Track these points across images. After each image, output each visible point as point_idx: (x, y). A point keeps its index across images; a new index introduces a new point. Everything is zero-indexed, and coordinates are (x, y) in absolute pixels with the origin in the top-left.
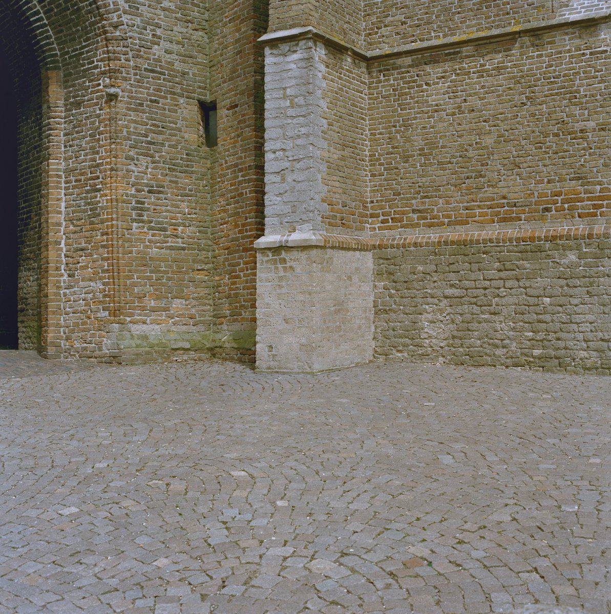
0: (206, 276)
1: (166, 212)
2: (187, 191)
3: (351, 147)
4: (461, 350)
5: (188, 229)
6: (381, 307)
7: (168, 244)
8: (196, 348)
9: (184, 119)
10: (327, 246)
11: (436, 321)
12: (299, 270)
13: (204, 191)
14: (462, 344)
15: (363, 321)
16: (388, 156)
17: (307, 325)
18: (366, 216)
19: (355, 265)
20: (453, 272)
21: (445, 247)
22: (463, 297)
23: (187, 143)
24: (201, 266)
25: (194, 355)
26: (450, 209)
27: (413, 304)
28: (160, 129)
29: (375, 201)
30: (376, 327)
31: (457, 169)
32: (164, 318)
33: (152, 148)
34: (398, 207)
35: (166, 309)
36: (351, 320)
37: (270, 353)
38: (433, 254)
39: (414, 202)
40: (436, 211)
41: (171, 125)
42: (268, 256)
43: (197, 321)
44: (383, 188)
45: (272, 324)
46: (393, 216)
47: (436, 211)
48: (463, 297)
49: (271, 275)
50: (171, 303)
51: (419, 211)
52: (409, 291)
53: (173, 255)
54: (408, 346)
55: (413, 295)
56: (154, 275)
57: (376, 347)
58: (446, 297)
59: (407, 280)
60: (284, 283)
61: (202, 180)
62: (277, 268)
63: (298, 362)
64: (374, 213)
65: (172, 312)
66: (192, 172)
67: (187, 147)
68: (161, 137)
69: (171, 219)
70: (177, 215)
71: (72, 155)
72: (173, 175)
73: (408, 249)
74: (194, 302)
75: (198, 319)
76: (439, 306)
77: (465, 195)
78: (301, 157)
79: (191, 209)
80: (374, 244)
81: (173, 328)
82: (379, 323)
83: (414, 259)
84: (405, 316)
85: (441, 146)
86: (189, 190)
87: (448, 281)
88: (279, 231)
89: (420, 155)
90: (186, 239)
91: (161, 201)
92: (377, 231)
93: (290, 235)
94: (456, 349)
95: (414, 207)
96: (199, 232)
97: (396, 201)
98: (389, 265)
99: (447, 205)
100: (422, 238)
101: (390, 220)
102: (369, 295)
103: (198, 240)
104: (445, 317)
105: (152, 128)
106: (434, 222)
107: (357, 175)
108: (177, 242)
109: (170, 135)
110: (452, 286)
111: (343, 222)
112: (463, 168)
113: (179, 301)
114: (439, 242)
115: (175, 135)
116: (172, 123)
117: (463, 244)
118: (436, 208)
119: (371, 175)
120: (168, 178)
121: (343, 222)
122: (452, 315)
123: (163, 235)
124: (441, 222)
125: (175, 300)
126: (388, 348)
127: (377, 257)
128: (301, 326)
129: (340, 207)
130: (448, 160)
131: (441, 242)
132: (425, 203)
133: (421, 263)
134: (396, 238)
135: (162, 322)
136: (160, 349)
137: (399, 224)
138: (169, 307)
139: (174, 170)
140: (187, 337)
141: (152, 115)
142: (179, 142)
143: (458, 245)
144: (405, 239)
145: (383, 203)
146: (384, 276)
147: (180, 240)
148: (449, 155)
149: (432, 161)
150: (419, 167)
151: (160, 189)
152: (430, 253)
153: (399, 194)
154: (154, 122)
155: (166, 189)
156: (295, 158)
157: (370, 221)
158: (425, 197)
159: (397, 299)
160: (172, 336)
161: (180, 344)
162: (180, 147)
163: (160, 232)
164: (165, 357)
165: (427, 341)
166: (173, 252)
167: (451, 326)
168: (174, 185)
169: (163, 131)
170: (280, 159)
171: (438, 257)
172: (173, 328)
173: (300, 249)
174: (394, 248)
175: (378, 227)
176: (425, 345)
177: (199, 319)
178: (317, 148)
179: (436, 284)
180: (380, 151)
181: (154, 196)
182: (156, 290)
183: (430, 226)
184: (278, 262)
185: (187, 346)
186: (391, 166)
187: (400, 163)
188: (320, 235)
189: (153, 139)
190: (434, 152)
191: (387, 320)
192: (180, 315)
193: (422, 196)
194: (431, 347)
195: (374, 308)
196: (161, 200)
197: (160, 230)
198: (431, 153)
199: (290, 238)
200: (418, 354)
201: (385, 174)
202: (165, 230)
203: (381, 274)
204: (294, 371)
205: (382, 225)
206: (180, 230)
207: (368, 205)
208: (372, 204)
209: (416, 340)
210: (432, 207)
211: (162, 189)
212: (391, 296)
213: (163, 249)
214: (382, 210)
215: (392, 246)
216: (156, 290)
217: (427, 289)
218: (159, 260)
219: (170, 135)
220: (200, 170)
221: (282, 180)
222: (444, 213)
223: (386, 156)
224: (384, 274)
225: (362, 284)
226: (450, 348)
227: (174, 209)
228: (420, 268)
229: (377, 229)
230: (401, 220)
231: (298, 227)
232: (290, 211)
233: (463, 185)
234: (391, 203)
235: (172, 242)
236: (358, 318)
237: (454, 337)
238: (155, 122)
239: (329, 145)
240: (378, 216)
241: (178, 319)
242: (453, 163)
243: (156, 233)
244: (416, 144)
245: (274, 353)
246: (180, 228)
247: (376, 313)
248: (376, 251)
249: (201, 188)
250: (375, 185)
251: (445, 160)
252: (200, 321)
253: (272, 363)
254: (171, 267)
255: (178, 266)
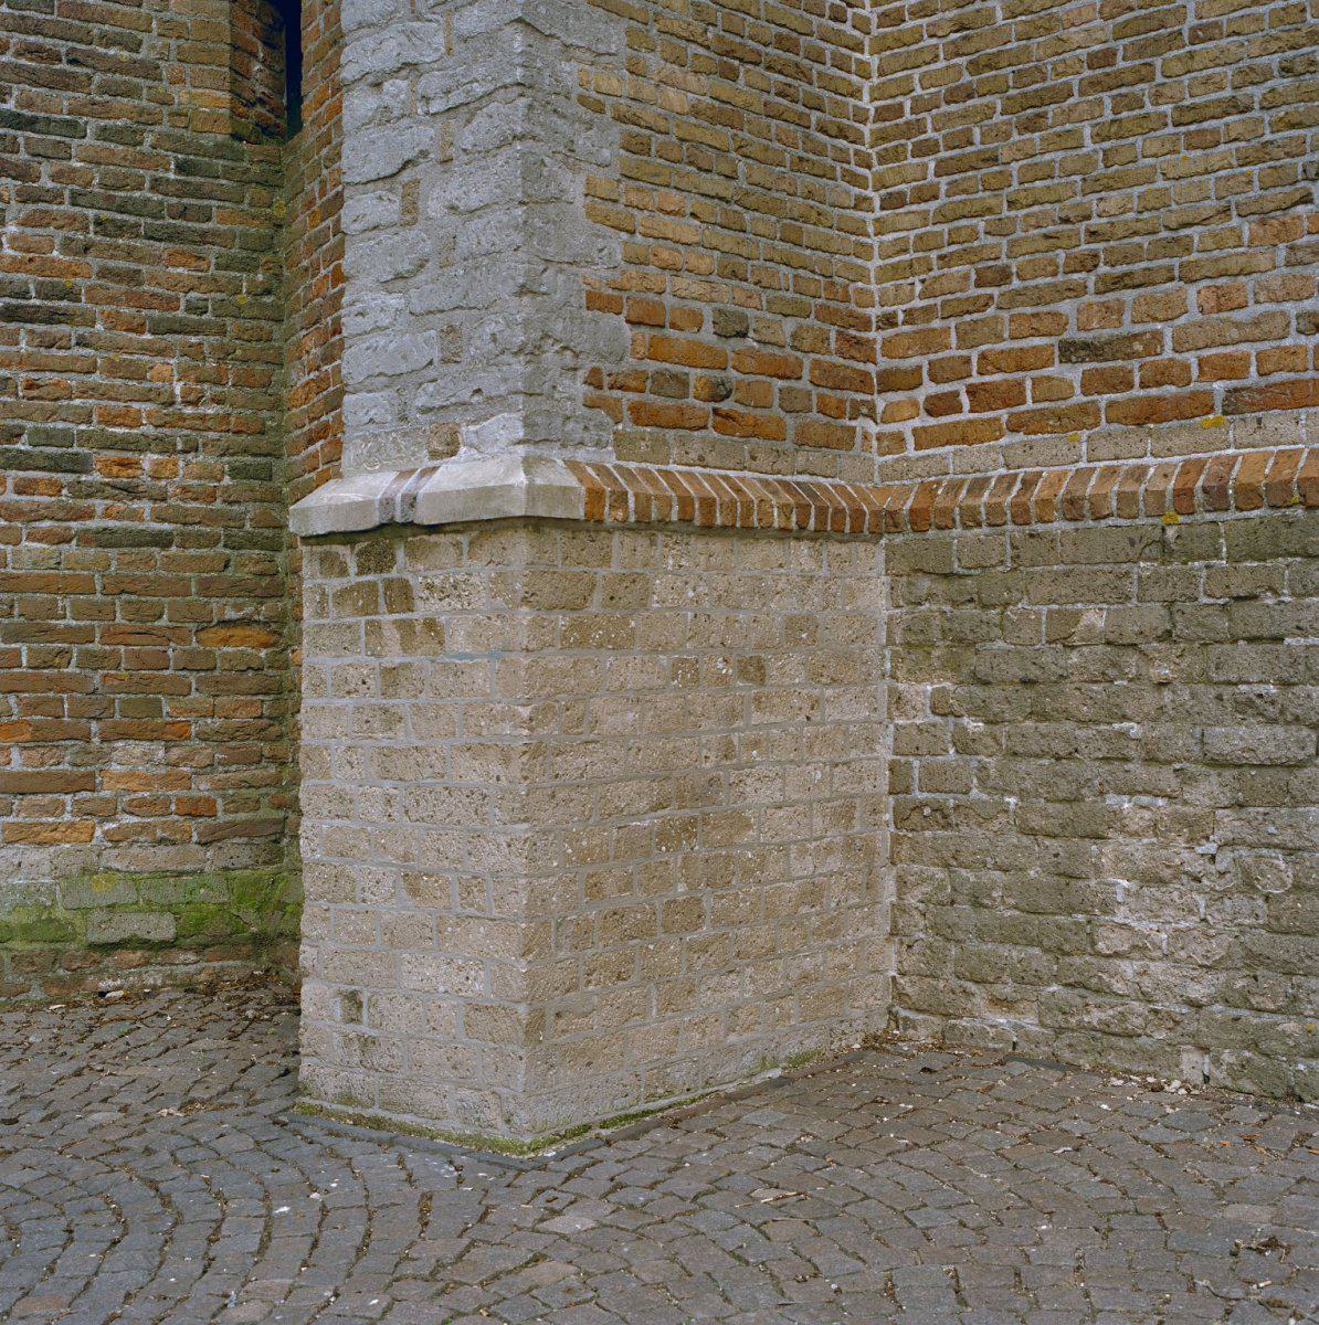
0: (265, 645)
1: (83, 394)
2: (180, 314)
3: (769, 68)
4: (1290, 1026)
5: (181, 464)
6: (922, 796)
7: (92, 524)
8: (201, 939)
9: (170, 29)
10: (608, 520)
11: (1167, 873)
12: (460, 636)
13: (256, 312)
14: (1295, 998)
15: (834, 863)
16: (953, 107)
17: (495, 913)
18: (863, 382)
19: (783, 607)
20: (1251, 640)
21: (1209, 517)
22: (1300, 765)
23: (182, 121)
24: (238, 607)
25: (192, 968)
26: (1235, 333)
27: (1064, 789)
28: (64, 66)
29: (901, 317)
30: (902, 882)
31: (1268, 137)
32: (67, 817)
33: (21, 140)
34: (1000, 338)
35: (87, 783)
36: (762, 867)
37: (350, 1028)
38: (1155, 551)
39: (1066, 307)
40: (1169, 343)
41: (112, 52)
42: (343, 572)
43: (220, 827)
44: (934, 255)
45: (358, 895)
46: (976, 379)
47: (1169, 343)
48: (1300, 765)
49: (359, 662)
50: (104, 757)
51: (1092, 350)
52: (1042, 726)
53: (114, 563)
54: (1038, 980)
55: (1059, 747)
56: (25, 648)
57: (903, 974)
58: (1217, 763)
59: (1034, 672)
60: (401, 703)
61: (248, 266)
62: (375, 629)
63: (459, 1086)
64: (898, 370)
65: (106, 794)
66: (204, 240)
67: (180, 139)
68: (64, 100)
69: (107, 423)
70: (136, 406)
71: (809, 394)
72: (117, 247)
73: (1040, 528)
74: (205, 753)
75: (222, 817)
76: (1185, 803)
77: (1308, 258)
78: (479, 89)
79: (199, 381)
80: (895, 507)
81: (112, 858)
82: (916, 867)
83: (1067, 574)
84: (1026, 840)
85: (1193, 30)
86: (190, 308)
87: (1229, 683)
88: (394, 454)
89: (1095, 84)
90: (172, 501)
91: (61, 353)
92: (911, 452)
93: (435, 469)
94: (1266, 1018)
95: (1071, 333)
96: (235, 472)
97: (991, 311)
98: (954, 603)
99: (1224, 315)
100: (1102, 476)
101: (965, 400)
102: (870, 741)
103: (231, 503)
104: (1213, 858)
105: (23, 61)
106: (1160, 399)
107: (810, 195)
108: (135, 515)
109: (104, 89)
110: (1246, 706)
111: (725, 406)
112: (1299, 125)
113: (137, 748)
114: (1184, 494)
115: (131, 92)
116: (115, 43)
117: (1297, 497)
118: (1168, 333)
119: (882, 200)
120: (93, 261)
121: (725, 406)
122: (1244, 852)
123: (70, 486)
124: (1194, 395)
125: (120, 744)
126: (954, 982)
127: (904, 567)
128: (471, 911)
129: (707, 335)
130: (1227, 93)
131: (1189, 493)
132: (1120, 312)
133: (1094, 596)
134: (988, 480)
135: (57, 835)
136: (37, 946)
137: (1003, 414)
138: (92, 775)
139: (121, 229)
140: (171, 892)
141: (27, 13)
142: (146, 120)
143: (1273, 507)
144: (1028, 484)
145: (936, 324)
146: (936, 653)
147: (145, 506)
148: (1229, 71)
149: (1149, 108)
150: (1089, 146)
151: (57, 303)
152: (1138, 547)
153: (1003, 276)
154: (32, 39)
155: (84, 304)
156: (455, 99)
157: (880, 405)
158: (1119, 282)
159: (991, 762)
160: (102, 892)
161: (133, 925)
162: (149, 139)
163: (55, 476)
164: (60, 979)
165: (1128, 968)
166: (112, 553)
167: (1240, 901)
168: (124, 287)
169: (74, 76)
170: (396, 113)
171: (1176, 565)
172: (112, 858)
173: (463, 539)
174: (979, 525)
175: (915, 431)
176: (1118, 987)
177: (231, 817)
178: (554, 45)
179: (1167, 695)
180: (919, 91)
181: (32, 332)
182: (32, 707)
183: (1145, 415)
184: (381, 600)
185: (164, 928)
186: (970, 149)
187: (1008, 135)
188: (573, 466)
189: (30, 105)
190: (1158, 62)
191: (947, 855)
192: (142, 803)
193: (1101, 279)
194: (1147, 998)
195: (891, 799)
196: (60, 348)
197: (55, 465)
198: (1144, 71)
199: (429, 486)
200: (1081, 1027)
201: (943, 188)
202: (78, 465)
203: (920, 645)
204: (443, 1125)
205: (932, 421)
206: (146, 466)
207: (872, 335)
208: (890, 332)
209: (1077, 960)
210: (1151, 326)
211: (64, 303)
212: (965, 746)
213: (69, 541)
214: (932, 357)
215: (971, 519)
216: (32, 707)
217: (1124, 718)
218: (46, 585)
219: (104, 89)
220: (239, 228)
221: (406, 211)
222: (1206, 353)
223: (944, 108)
224: (933, 645)
225: (829, 692)
226: (1234, 1012)
227: (118, 382)
228: (1095, 618)
229: (911, 441)
230: (1012, 396)
231: (467, 431)
232: (436, 356)
233: (1301, 209)
234: (967, 318)
235: (107, 514)
236: (803, 852)
237: (1254, 959)
238: (40, 39)
239: (636, 40)
240: (911, 380)
241: (135, 819)
242: (1248, 109)
243: (35, 481)
244: (1074, 34)
245: (364, 1029)
246: (148, 460)
247: (900, 820)
248: (899, 539)
249: (243, 298)
250: (902, 245)
251: (1214, 96)
252: (233, 824)
253: (358, 1076)
254: (100, 612)
255: (135, 611)
